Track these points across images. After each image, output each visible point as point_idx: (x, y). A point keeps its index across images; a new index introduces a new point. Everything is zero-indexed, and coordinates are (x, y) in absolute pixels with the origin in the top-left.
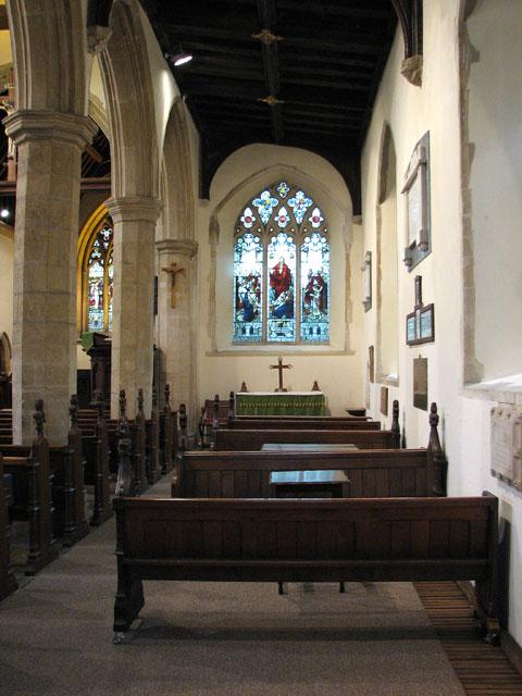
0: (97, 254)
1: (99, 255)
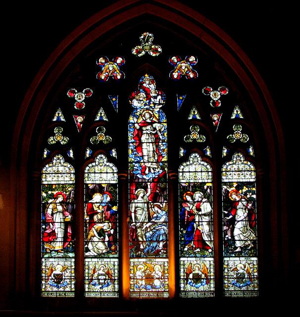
0: (58, 138)
1: (64, 140)
